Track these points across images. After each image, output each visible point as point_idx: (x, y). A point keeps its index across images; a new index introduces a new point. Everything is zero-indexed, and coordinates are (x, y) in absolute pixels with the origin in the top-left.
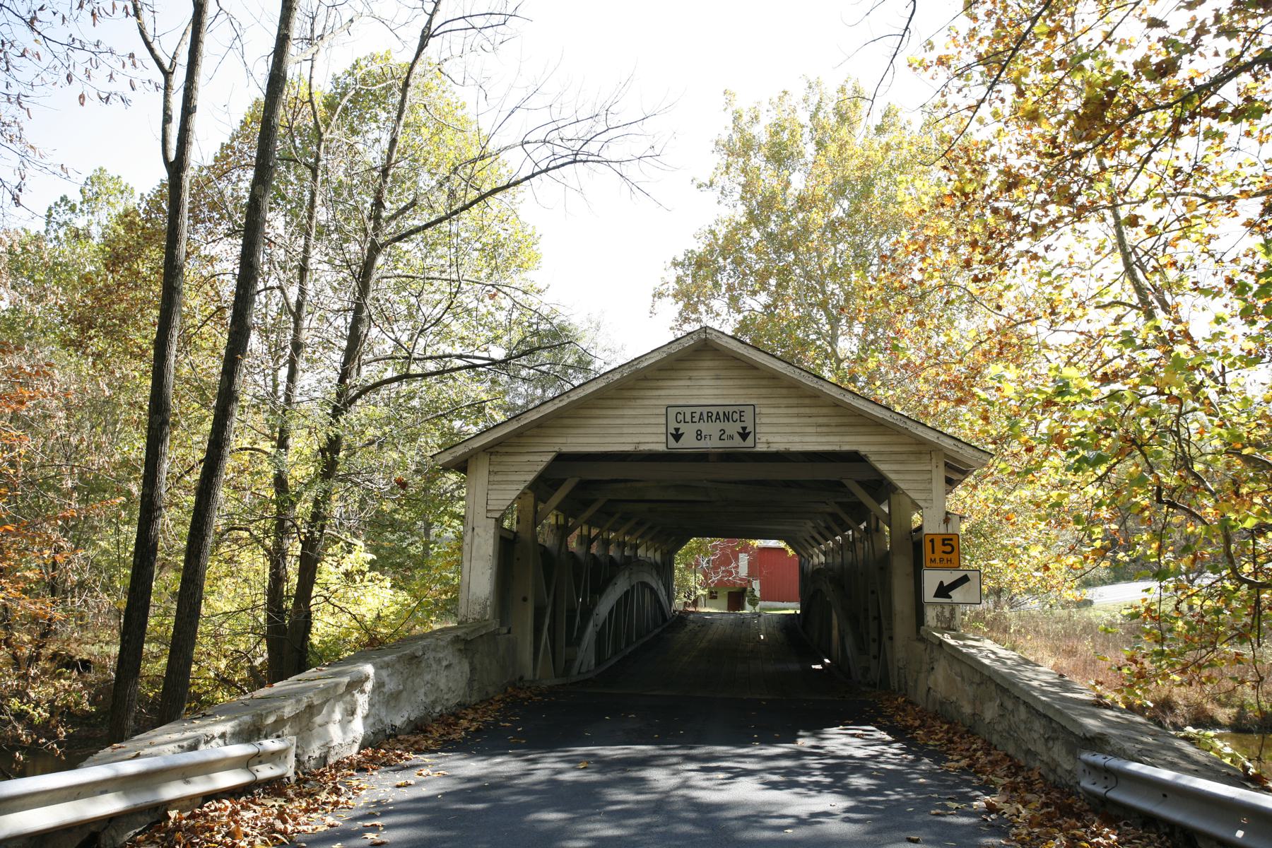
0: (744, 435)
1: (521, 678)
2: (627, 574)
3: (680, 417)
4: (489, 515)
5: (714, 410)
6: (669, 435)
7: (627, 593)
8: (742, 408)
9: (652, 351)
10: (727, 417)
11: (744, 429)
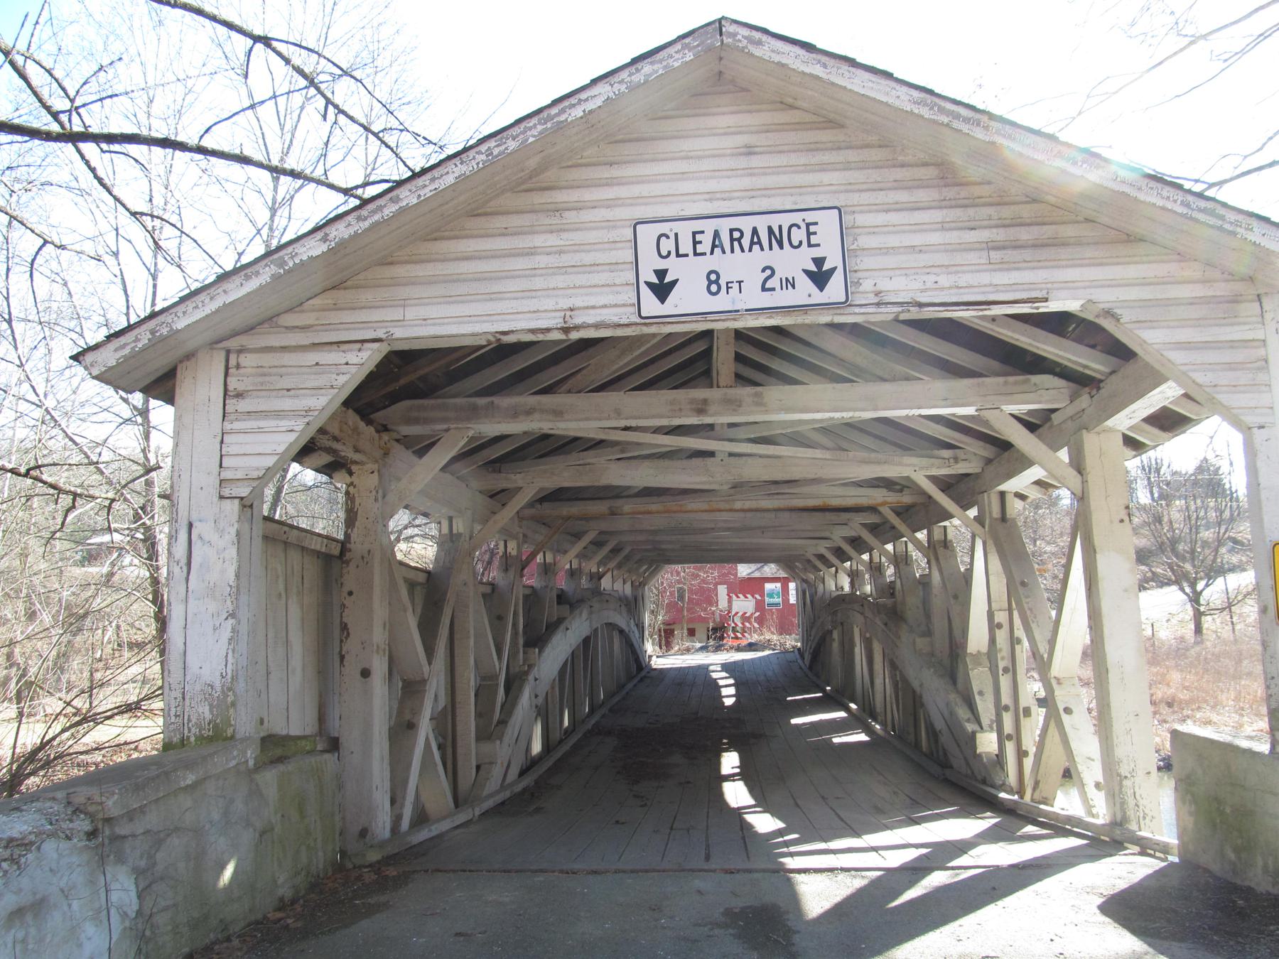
0: (820, 277)
1: (364, 833)
2: (585, 615)
3: (667, 245)
4: (226, 492)
5: (746, 224)
6: (644, 288)
7: (586, 641)
8: (810, 217)
9: (595, 82)
10: (776, 238)
11: (819, 262)
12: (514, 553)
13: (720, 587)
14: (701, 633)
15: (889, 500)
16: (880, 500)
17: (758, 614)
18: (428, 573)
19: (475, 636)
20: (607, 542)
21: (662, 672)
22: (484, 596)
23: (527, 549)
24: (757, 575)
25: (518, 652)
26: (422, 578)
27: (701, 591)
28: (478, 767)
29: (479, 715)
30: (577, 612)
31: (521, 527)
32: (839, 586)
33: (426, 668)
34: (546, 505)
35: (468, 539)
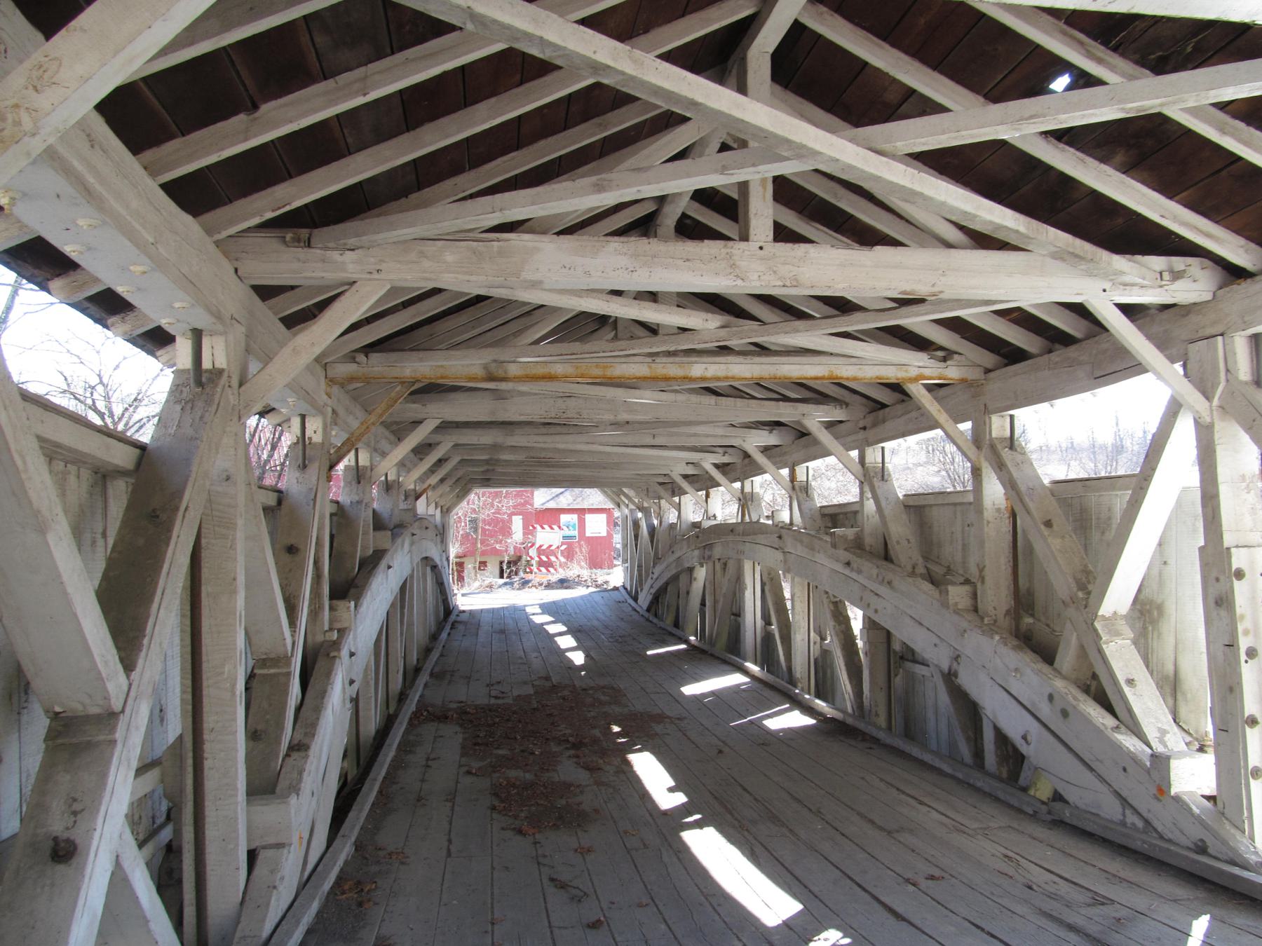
12: (317, 438)
13: (514, 518)
14: (493, 568)
15: (927, 372)
16: (913, 372)
17: (564, 547)
18: (142, 448)
19: (247, 587)
20: (438, 444)
21: (474, 618)
22: (267, 510)
23: (338, 437)
24: (552, 505)
25: (321, 607)
26: (122, 457)
27: (494, 521)
28: (252, 856)
29: (253, 735)
30: (399, 541)
31: (329, 396)
32: (711, 514)
33: (116, 682)
34: (375, 357)
35: (235, 382)
